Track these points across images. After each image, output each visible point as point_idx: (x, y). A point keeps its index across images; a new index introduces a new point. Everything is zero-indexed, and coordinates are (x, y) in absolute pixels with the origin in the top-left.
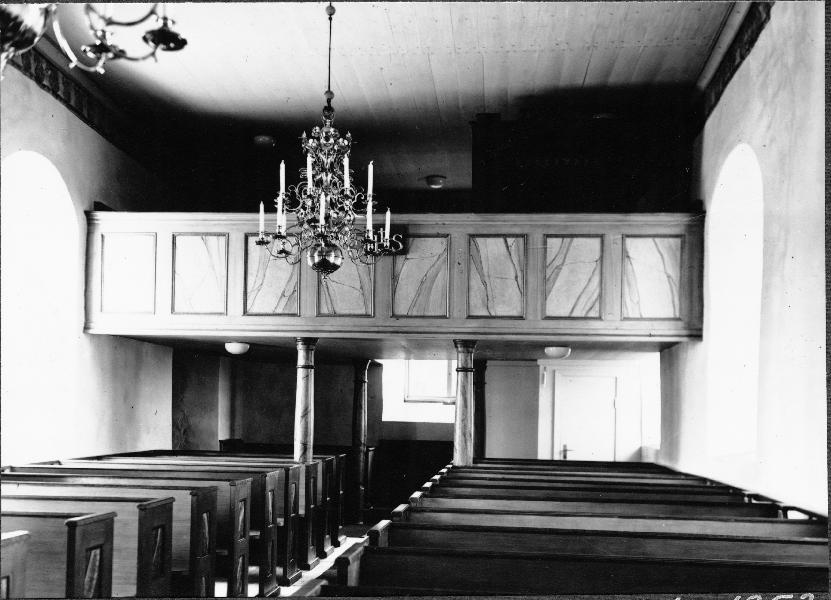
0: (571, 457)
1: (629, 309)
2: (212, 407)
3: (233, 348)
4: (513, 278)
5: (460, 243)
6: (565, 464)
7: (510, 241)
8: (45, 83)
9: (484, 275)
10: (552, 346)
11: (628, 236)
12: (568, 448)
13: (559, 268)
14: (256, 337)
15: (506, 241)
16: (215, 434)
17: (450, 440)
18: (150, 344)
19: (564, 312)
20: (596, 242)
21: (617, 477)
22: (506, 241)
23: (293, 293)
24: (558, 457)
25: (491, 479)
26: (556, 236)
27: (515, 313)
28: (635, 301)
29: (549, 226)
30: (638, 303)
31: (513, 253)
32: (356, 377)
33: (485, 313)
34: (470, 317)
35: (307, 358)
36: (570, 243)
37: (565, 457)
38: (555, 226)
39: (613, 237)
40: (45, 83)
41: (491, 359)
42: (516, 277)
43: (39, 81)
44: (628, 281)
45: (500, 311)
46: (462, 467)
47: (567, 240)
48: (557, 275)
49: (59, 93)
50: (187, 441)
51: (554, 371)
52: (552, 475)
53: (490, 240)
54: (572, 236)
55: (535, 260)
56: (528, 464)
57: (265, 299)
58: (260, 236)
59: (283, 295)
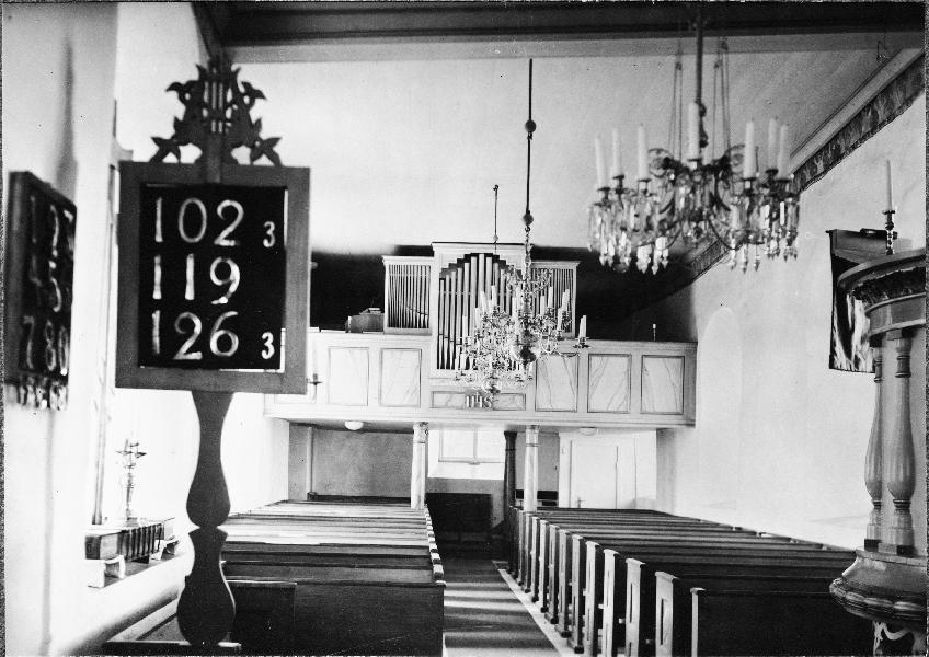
5: (636, 359)
24: (574, 506)
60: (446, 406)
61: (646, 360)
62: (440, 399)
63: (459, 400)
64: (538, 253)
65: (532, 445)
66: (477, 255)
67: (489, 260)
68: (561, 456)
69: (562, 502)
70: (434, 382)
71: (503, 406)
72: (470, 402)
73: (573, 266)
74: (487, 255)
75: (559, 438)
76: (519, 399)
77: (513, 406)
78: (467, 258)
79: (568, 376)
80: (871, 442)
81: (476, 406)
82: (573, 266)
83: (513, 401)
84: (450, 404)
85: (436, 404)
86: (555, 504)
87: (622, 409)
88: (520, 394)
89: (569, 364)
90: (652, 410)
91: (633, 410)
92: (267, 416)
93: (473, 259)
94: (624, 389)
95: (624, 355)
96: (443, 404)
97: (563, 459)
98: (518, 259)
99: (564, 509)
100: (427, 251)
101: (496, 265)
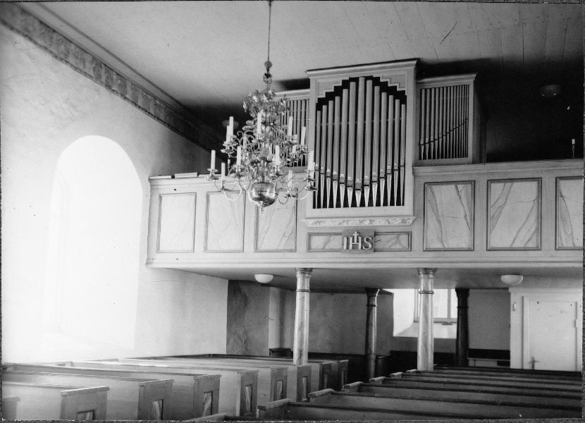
0: (538, 367)
1: (564, 239)
2: (263, 323)
3: (260, 278)
4: (463, 217)
5: (549, 183)
6: (533, 372)
7: (460, 187)
8: (114, 88)
9: (438, 216)
10: (506, 274)
11: (562, 178)
12: (536, 359)
13: (501, 207)
14: (283, 269)
15: (457, 188)
16: (265, 344)
17: (506, 349)
18: (218, 279)
19: (507, 244)
20: (534, 185)
21: (533, 382)
22: (457, 188)
23: (291, 235)
24: (527, 367)
25: (476, 384)
26: (499, 181)
27: (464, 246)
28: (569, 233)
29: (492, 173)
30: (571, 234)
31: (462, 197)
32: (369, 301)
33: (438, 246)
34: (427, 250)
35: (303, 284)
36: (511, 187)
37: (533, 366)
38: (498, 173)
39: (549, 183)
40: (114, 88)
41: (537, 277)
42: (466, 216)
43: (108, 87)
44: (562, 217)
45: (452, 244)
46: (424, 372)
47: (508, 184)
48: (500, 212)
49: (127, 96)
50: (246, 349)
51: (523, 297)
52: (497, 380)
53: (444, 187)
54: (512, 180)
55: (480, 200)
56: (502, 372)
57: (271, 239)
58: (288, 192)
59: (284, 235)
60: (323, 250)
61: (562, 183)
62: (318, 242)
63: (336, 242)
64: (424, 69)
65: (303, 291)
66: (356, 80)
67: (369, 83)
68: (512, 312)
69: (515, 363)
70: (310, 223)
71: (387, 246)
72: (348, 244)
73: (469, 80)
74: (367, 78)
75: (509, 294)
76: (404, 238)
77: (398, 246)
78: (346, 84)
79: (462, 210)
80: (237, 360)
81: (355, 247)
82: (469, 80)
83: (398, 241)
84: (327, 247)
85: (314, 246)
86: (508, 364)
87: (531, 245)
88: (405, 233)
89: (462, 194)
90: (570, 245)
91: (545, 245)
92: (150, 266)
93: (352, 85)
94: (532, 224)
95: (533, 179)
96: (321, 247)
97: (515, 318)
98: (404, 79)
99: (522, 372)
100: (303, 84)
101: (377, 89)
